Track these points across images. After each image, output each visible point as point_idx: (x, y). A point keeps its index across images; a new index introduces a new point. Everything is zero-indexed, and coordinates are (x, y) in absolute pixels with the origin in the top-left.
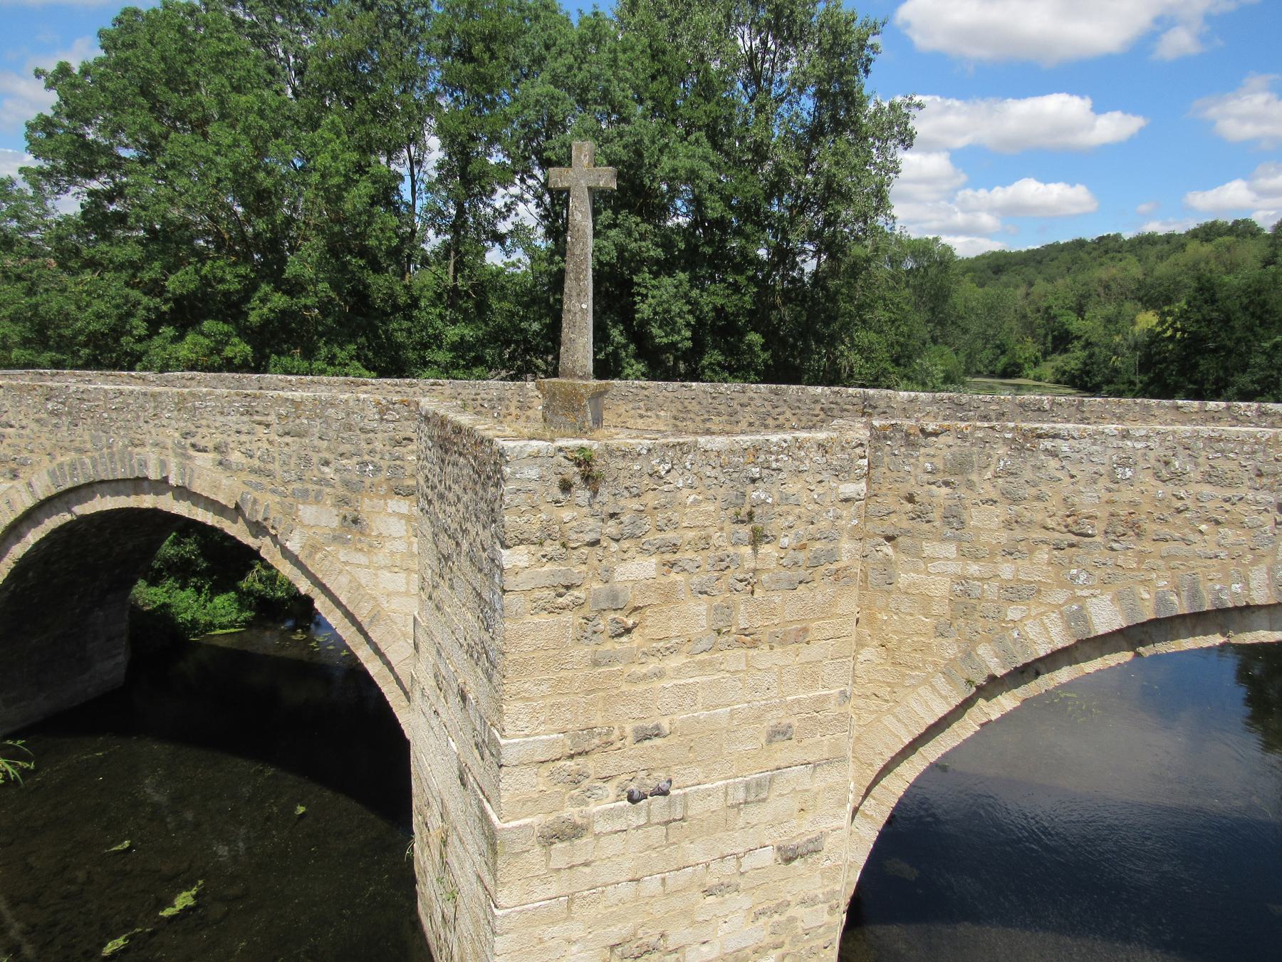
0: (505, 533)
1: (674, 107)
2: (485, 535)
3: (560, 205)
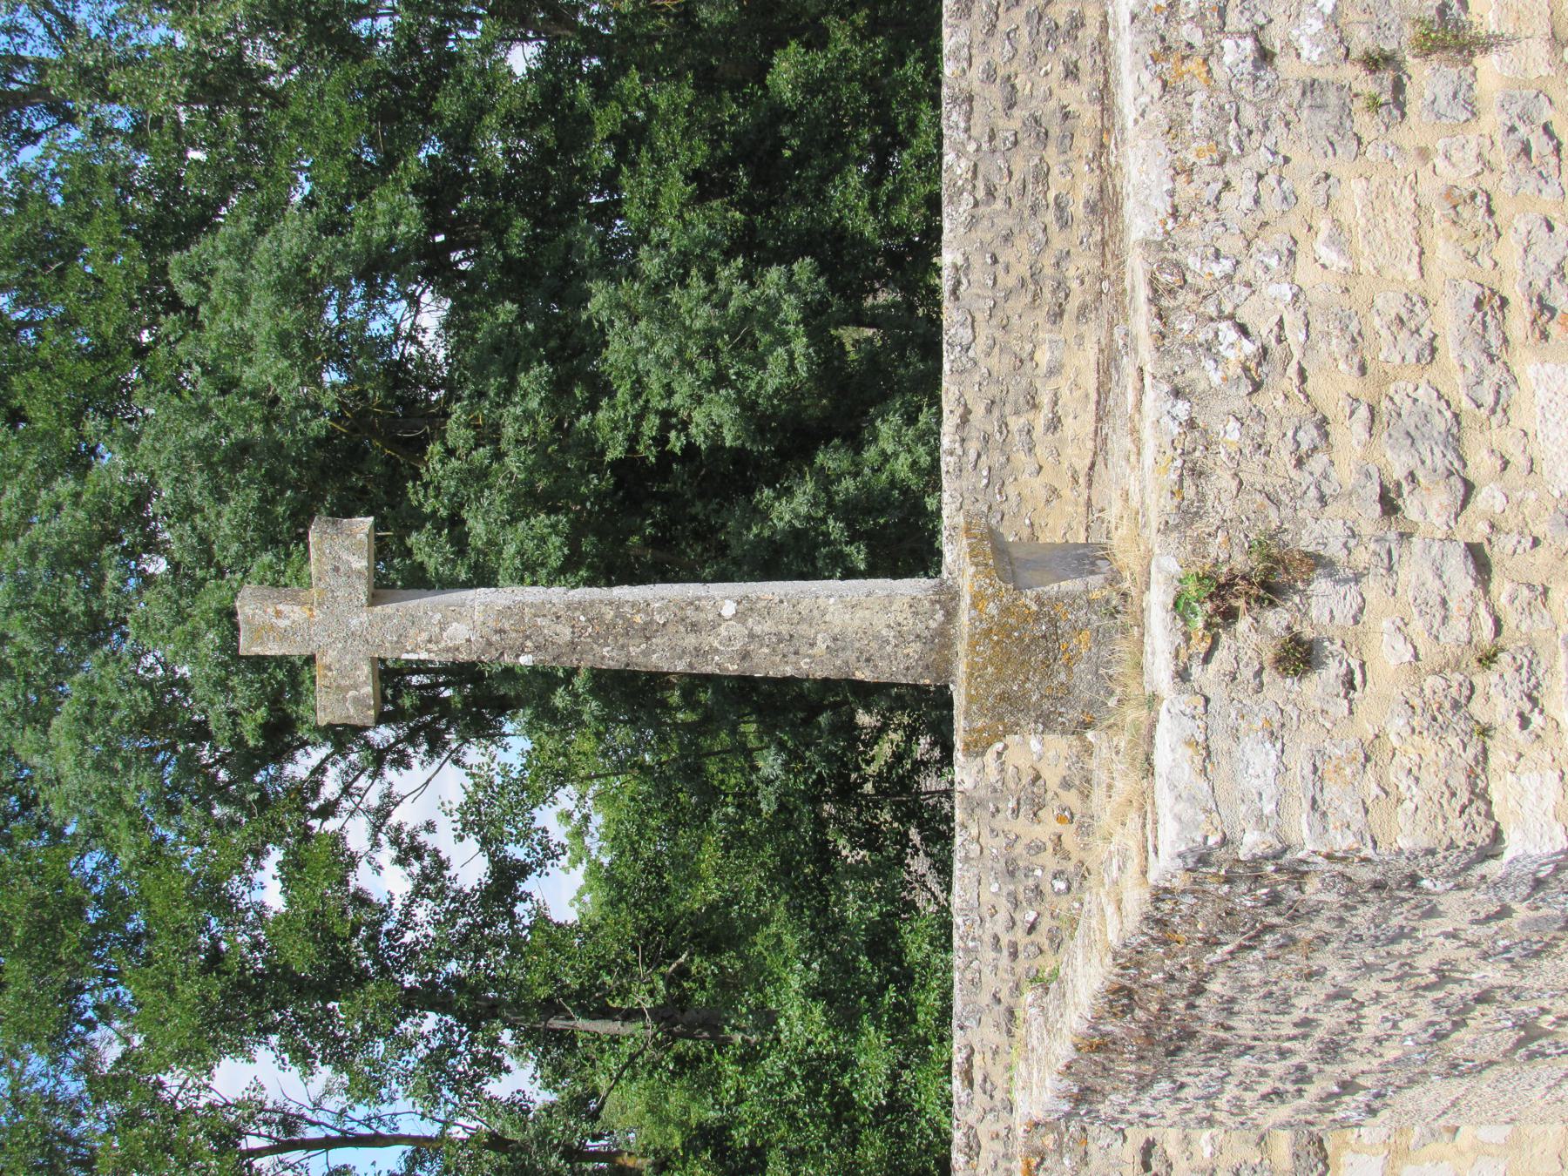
0: (1452, 845)
1: (101, 353)
2: (1456, 909)
3: (398, 694)
